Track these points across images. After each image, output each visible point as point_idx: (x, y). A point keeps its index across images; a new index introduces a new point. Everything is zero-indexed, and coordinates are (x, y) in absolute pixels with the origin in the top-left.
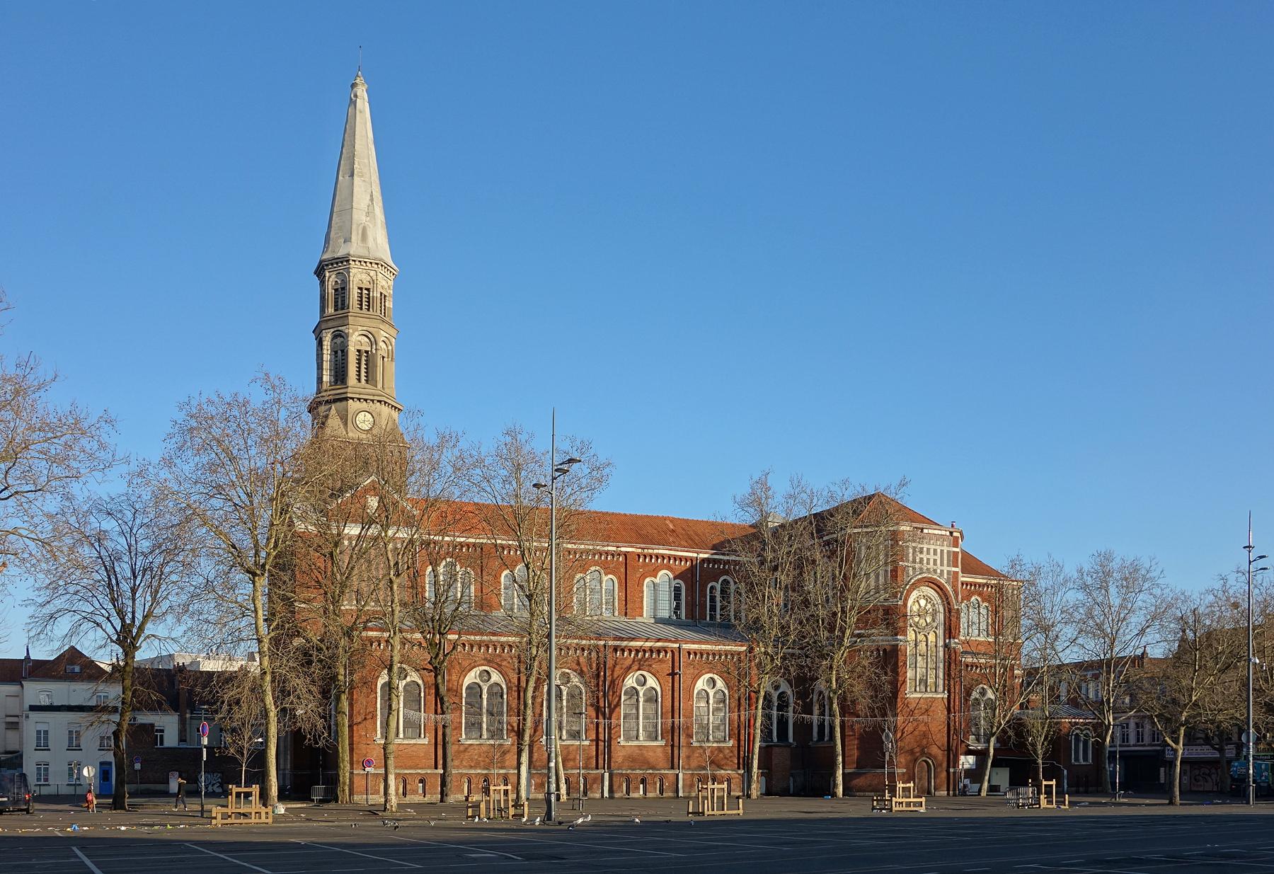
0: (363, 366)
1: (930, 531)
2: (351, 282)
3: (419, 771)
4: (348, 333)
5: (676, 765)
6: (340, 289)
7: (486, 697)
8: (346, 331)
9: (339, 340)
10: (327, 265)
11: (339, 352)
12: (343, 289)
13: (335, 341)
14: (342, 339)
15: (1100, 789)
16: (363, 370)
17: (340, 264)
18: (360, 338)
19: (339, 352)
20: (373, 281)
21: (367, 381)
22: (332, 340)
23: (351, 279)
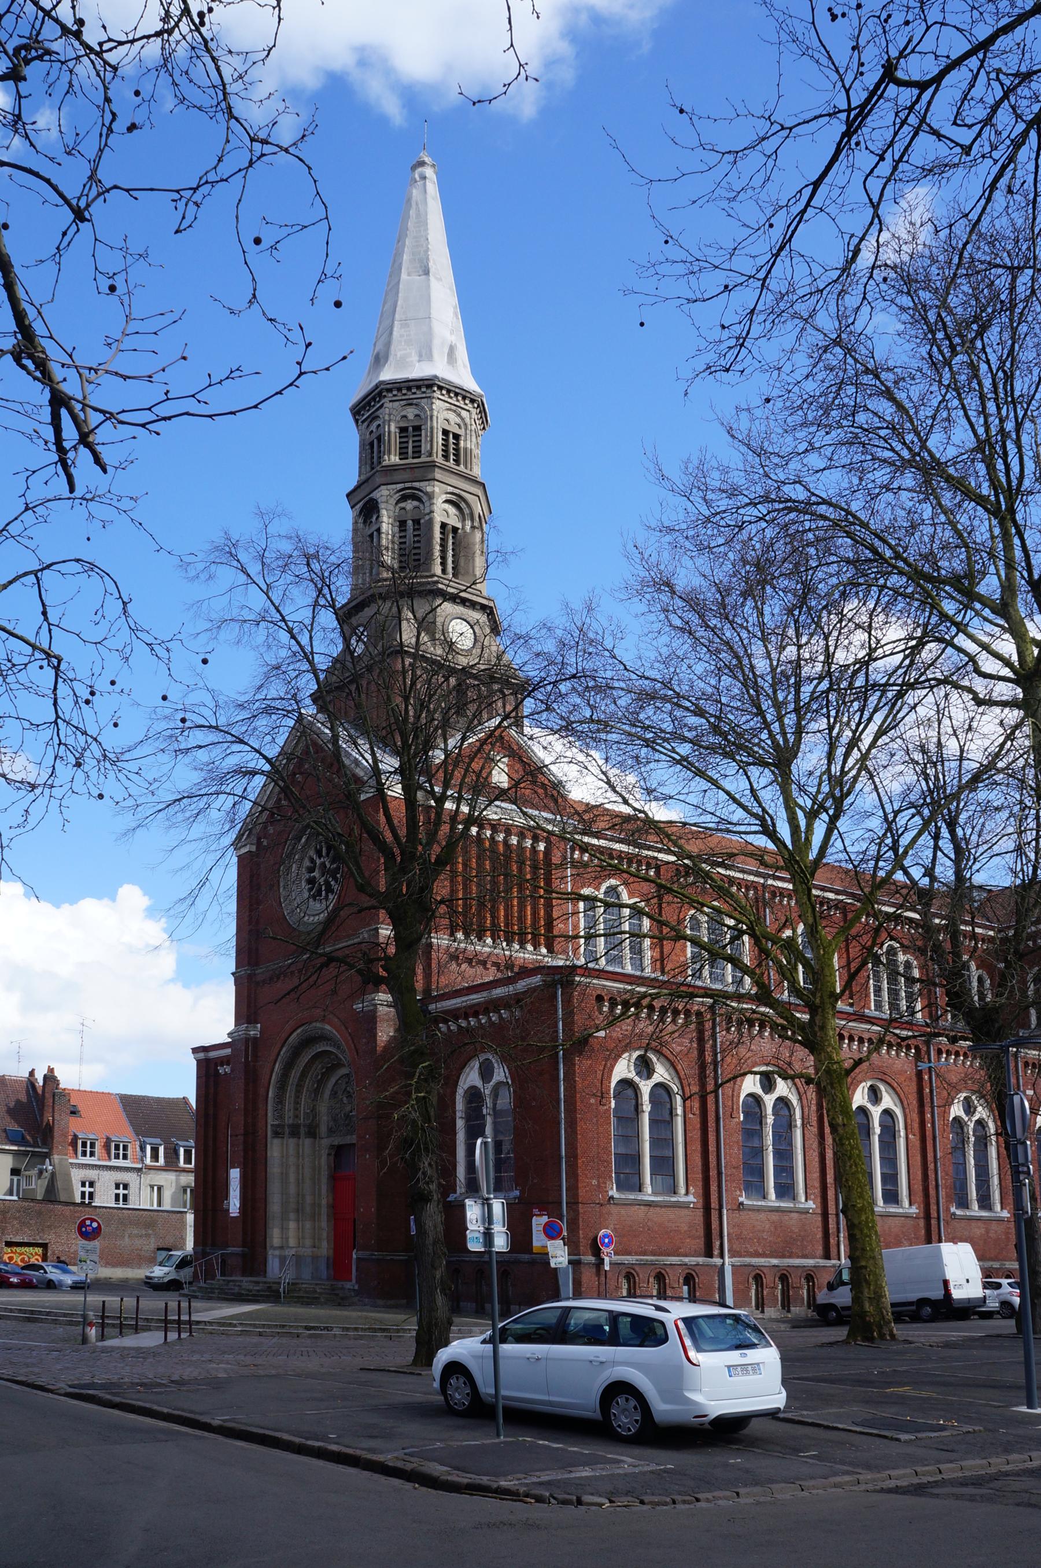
0: (450, 553)
1: (775, 883)
2: (435, 418)
3: (686, 1260)
4: (433, 492)
5: (833, 1251)
6: (411, 429)
7: (649, 1109)
8: (429, 489)
9: (410, 505)
10: (440, 388)
11: (410, 523)
12: (417, 429)
13: (402, 505)
14: (416, 503)
15: (201, 1055)
16: (450, 560)
17: (414, 390)
18: (447, 506)
19: (410, 523)
20: (466, 424)
21: (454, 575)
22: (396, 504)
23: (435, 413)
